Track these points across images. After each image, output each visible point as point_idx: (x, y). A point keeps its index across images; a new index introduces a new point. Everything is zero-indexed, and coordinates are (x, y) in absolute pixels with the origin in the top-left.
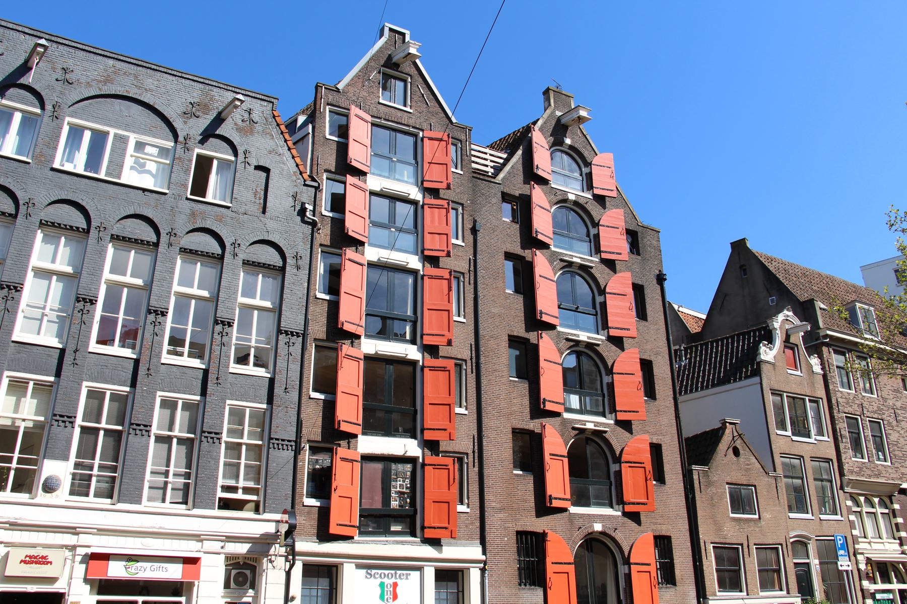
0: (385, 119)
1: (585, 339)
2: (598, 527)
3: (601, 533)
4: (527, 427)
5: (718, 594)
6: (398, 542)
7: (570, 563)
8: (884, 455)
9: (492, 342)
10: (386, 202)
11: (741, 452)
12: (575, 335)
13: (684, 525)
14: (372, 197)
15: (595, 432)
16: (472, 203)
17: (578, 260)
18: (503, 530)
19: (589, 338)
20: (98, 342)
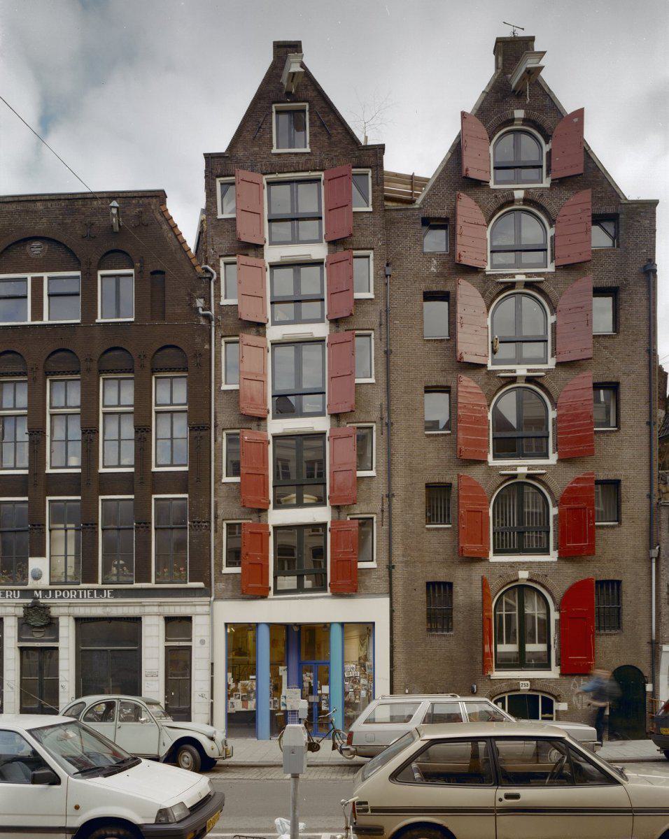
3: (529, 580)
4: (444, 481)
10: (289, 272)
15: (529, 476)
17: (523, 278)
19: (529, 370)
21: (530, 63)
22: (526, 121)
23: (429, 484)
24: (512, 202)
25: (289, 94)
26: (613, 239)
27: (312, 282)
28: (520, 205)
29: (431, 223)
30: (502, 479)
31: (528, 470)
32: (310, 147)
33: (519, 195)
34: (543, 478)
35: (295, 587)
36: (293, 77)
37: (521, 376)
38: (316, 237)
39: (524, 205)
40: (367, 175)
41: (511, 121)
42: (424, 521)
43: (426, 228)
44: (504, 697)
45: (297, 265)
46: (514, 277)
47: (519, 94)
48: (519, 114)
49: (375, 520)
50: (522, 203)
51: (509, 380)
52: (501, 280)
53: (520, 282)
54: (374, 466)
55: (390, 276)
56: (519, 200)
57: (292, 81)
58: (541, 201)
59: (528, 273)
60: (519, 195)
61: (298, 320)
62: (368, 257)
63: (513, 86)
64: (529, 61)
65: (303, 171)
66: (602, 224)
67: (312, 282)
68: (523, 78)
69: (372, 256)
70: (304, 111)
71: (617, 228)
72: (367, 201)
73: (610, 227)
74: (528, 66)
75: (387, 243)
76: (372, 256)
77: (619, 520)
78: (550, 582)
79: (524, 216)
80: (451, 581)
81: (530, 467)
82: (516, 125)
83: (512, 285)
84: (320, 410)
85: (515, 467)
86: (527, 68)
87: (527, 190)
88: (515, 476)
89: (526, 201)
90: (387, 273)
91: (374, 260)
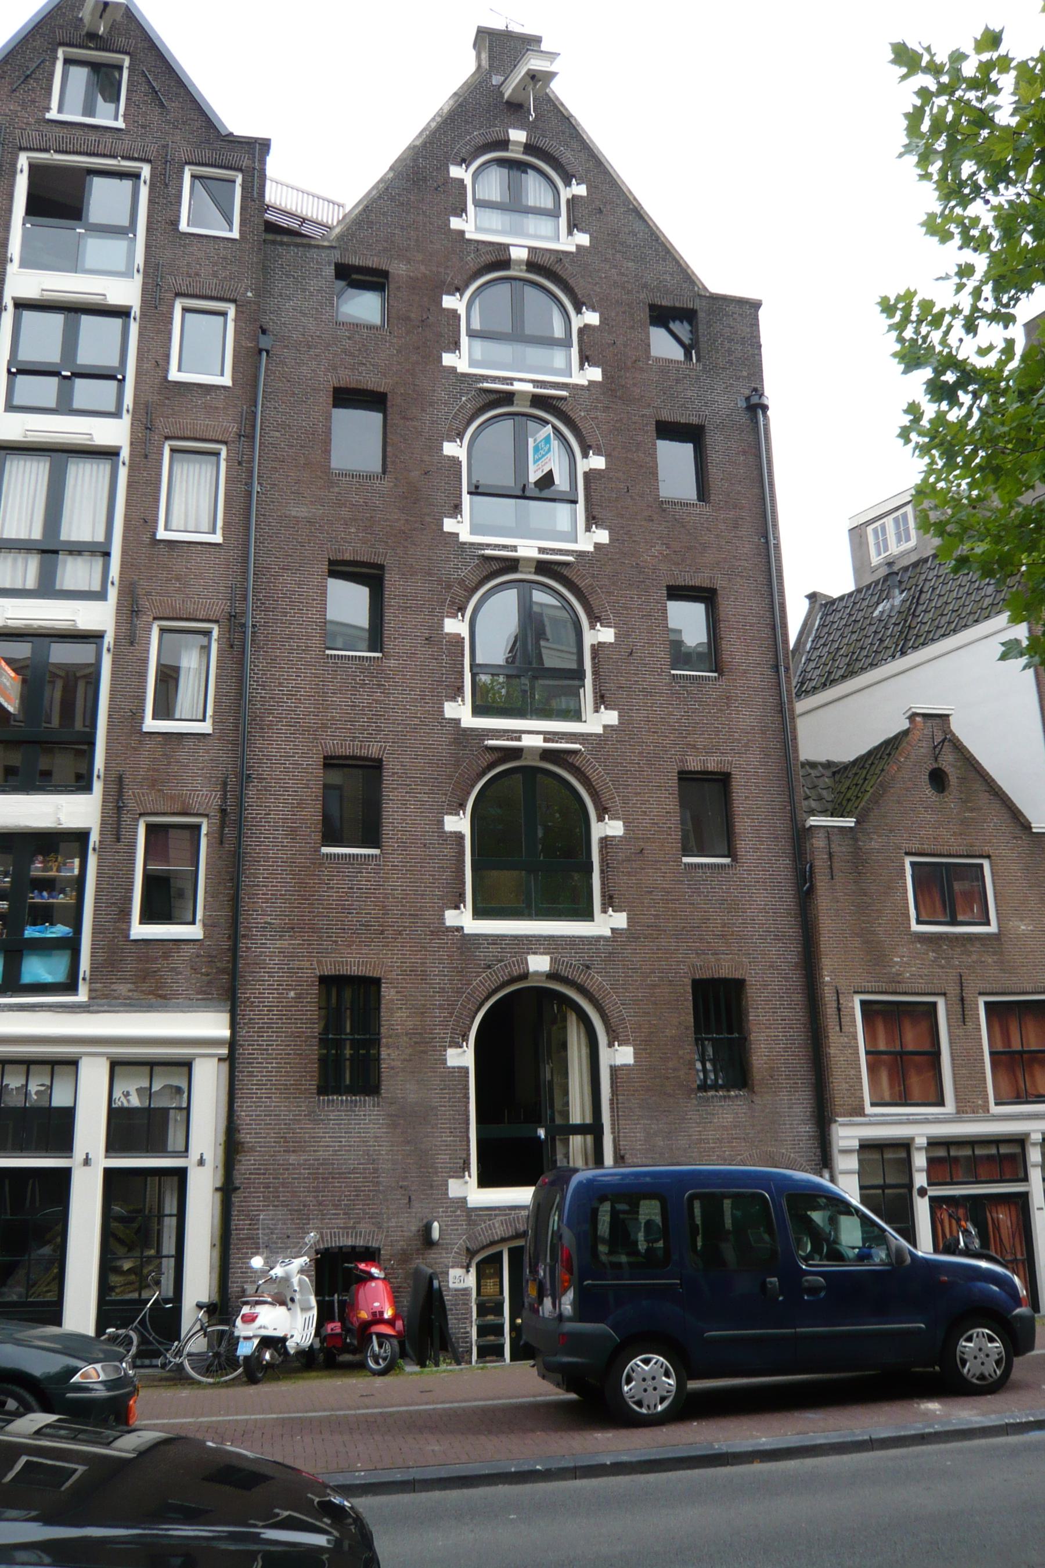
0: (123, 158)
1: (534, 554)
2: (539, 963)
3: (552, 976)
4: (364, 753)
5: (869, 1110)
6: (22, 1008)
7: (853, 1173)
8: (463, 616)
9: (287, 577)
10: (56, 321)
11: (953, 781)
12: (505, 547)
13: (788, 955)
14: (188, 315)
15: (547, 755)
16: (257, 295)
17: (529, 387)
18: (283, 972)
19: (542, 550)
20: (997, 1104)
21: (535, 63)
22: (529, 148)
23: (332, 757)
24: (505, 263)
25: (92, 36)
26: (687, 350)
27: (98, 343)
28: (521, 271)
29: (354, 276)
30: (489, 757)
31: (545, 740)
32: (125, 121)
33: (519, 254)
34: (577, 761)
35: (31, 583)
36: (104, 10)
37: (528, 560)
38: (122, 268)
39: (528, 271)
40: (234, 182)
41: (504, 144)
42: (318, 837)
43: (342, 284)
44: (501, 1253)
45: (74, 310)
46: (512, 384)
47: (515, 109)
48: (518, 135)
49: (204, 830)
50: (525, 268)
51: (493, 397)
52: (486, 385)
53: (523, 393)
54: (210, 712)
55: (267, 352)
56: (519, 262)
57: (101, 17)
58: (557, 268)
59: (538, 381)
60: (519, 254)
61: (64, 407)
62: (217, 454)
63: (506, 96)
64: (532, 61)
65: (104, 156)
66: (672, 326)
67: (98, 343)
68: (522, 87)
69: (224, 454)
70: (120, 68)
71: (694, 331)
72: (230, 223)
73: (682, 329)
74: (532, 67)
75: (262, 291)
76: (224, 454)
77: (731, 853)
78: (596, 981)
79: (529, 290)
80: (373, 750)
81: (549, 736)
82: (512, 151)
83: (508, 398)
84: (96, 587)
85: (517, 735)
86: (529, 70)
87: (532, 250)
88: (516, 753)
89: (532, 266)
90: (262, 346)
91: (236, 320)
